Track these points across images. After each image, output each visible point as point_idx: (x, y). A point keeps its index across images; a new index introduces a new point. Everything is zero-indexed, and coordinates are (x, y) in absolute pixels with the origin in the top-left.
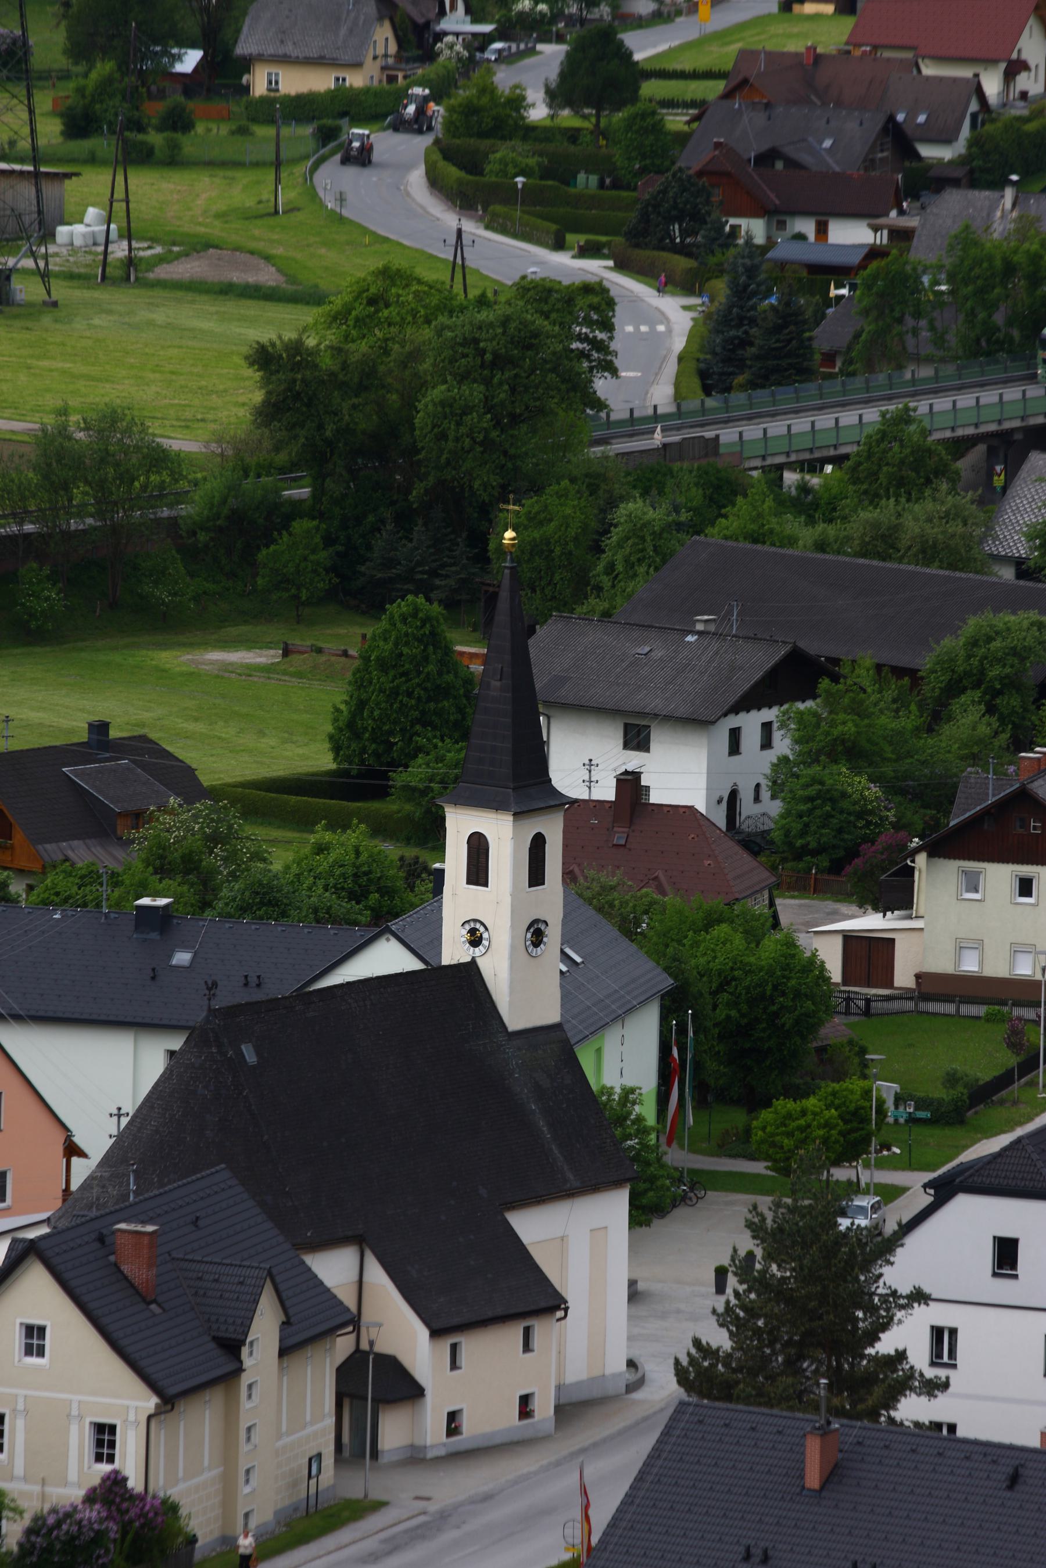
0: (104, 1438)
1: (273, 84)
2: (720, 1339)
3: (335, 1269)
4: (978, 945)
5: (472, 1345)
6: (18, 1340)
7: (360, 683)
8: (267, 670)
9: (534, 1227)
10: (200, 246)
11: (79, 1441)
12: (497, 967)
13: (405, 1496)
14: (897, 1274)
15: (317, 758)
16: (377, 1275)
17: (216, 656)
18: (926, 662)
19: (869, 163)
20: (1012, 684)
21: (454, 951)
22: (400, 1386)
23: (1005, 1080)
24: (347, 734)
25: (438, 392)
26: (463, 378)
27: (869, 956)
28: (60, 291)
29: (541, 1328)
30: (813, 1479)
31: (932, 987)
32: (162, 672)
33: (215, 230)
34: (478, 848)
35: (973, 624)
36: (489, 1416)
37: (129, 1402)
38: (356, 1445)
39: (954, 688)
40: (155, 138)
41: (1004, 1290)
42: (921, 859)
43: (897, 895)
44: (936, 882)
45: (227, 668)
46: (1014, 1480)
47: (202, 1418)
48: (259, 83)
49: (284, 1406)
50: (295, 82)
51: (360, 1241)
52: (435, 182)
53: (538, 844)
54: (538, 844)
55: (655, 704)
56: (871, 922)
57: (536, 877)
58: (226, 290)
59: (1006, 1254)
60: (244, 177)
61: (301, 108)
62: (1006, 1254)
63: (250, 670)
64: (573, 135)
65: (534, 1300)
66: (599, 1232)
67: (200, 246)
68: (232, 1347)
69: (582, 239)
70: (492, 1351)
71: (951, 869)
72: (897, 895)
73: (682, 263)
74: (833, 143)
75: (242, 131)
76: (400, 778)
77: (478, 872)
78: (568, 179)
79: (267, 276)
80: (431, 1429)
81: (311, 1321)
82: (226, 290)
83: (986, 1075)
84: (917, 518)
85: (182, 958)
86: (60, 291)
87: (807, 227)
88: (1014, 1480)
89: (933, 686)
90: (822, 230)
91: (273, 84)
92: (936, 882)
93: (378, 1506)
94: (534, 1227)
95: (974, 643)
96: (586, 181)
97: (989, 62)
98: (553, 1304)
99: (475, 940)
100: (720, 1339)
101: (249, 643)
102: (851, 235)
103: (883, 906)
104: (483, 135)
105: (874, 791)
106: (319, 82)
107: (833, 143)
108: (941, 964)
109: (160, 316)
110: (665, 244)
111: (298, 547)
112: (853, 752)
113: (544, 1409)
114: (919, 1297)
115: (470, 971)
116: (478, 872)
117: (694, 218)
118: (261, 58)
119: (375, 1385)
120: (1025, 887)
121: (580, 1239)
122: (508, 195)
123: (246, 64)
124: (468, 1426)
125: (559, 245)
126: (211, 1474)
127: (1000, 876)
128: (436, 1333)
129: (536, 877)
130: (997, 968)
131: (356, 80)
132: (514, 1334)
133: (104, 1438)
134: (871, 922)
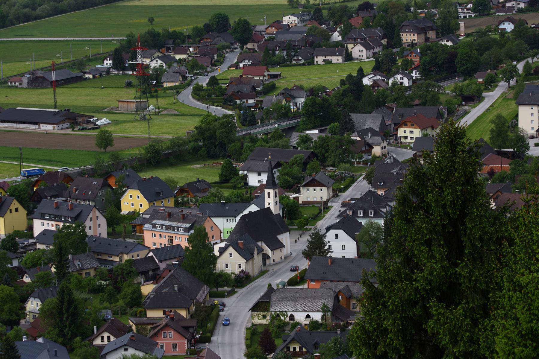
0: (240, 266)
1: (166, 85)
2: (307, 249)
3: (259, 243)
4: (310, 197)
5: (275, 252)
6: (229, 255)
7: (222, 169)
8: (203, 167)
9: (280, 237)
10: (166, 109)
11: (237, 266)
12: (272, 207)
13: (272, 270)
14: (326, 240)
15: (217, 179)
16: (264, 245)
17: (195, 166)
18: (289, 161)
19: (251, 92)
20: (300, 163)
21: (267, 206)
22: (269, 257)
23: (319, 213)
24: (221, 176)
25: (219, 130)
26: (222, 128)
27: (297, 199)
28: (152, 117)
29: (282, 249)
30: (330, 264)
31: (304, 203)
32: (190, 169)
33: (167, 106)
34: (269, 194)
35: (295, 156)
36: (278, 260)
37: (243, 261)
38: (264, 264)
39: (293, 164)
40: (154, 94)
41: (337, 240)
42: (301, 188)
43: (298, 191)
44: (303, 190)
45: (197, 167)
46: (352, 262)
47: (250, 262)
48: (165, 85)
49: (258, 259)
50: (170, 85)
51: (261, 241)
52: (193, 97)
53: (276, 192)
54: (276, 192)
55: (262, 170)
56: (296, 195)
57: (276, 197)
58: (172, 115)
59: (336, 236)
60: (167, 99)
61: (171, 88)
62: (336, 236)
63: (201, 167)
64: (209, 90)
65: (280, 246)
66: (286, 237)
67: (166, 109)
68: (252, 254)
69: (216, 104)
70: (277, 252)
71: (306, 189)
72: (298, 191)
73: (231, 107)
74: (246, 89)
75: (165, 92)
76: (230, 181)
77: (269, 197)
78: (211, 96)
79: (176, 112)
80: (272, 262)
81: (260, 250)
82: (172, 115)
83: (317, 213)
84: (280, 142)
85: (227, 208)
86: (152, 117)
87: (245, 101)
88: (352, 262)
89: (291, 164)
90: (247, 101)
91: (166, 85)
92: (303, 190)
93: (268, 271)
94: (280, 237)
95: (295, 158)
96: (213, 96)
97: (261, 76)
98: (283, 246)
99: (269, 204)
100: (307, 249)
101: (199, 164)
102: (251, 101)
103: (296, 193)
104: (199, 91)
105: (290, 179)
106: (173, 84)
107: (246, 89)
108: (305, 200)
109: (165, 119)
110: (228, 105)
111: (203, 151)
112: (287, 174)
113: (283, 258)
114: (329, 242)
115: (269, 207)
116: (269, 197)
117: (231, 101)
118: (165, 82)
119: (266, 257)
120: (315, 190)
121: (285, 238)
122: (206, 99)
123: (162, 83)
124: (275, 261)
125: (213, 105)
126: (251, 269)
127: (311, 189)
128: (271, 251)
129: (276, 197)
130: (312, 200)
131: (177, 84)
132: (279, 250)
133: (240, 266)
134: (296, 195)
